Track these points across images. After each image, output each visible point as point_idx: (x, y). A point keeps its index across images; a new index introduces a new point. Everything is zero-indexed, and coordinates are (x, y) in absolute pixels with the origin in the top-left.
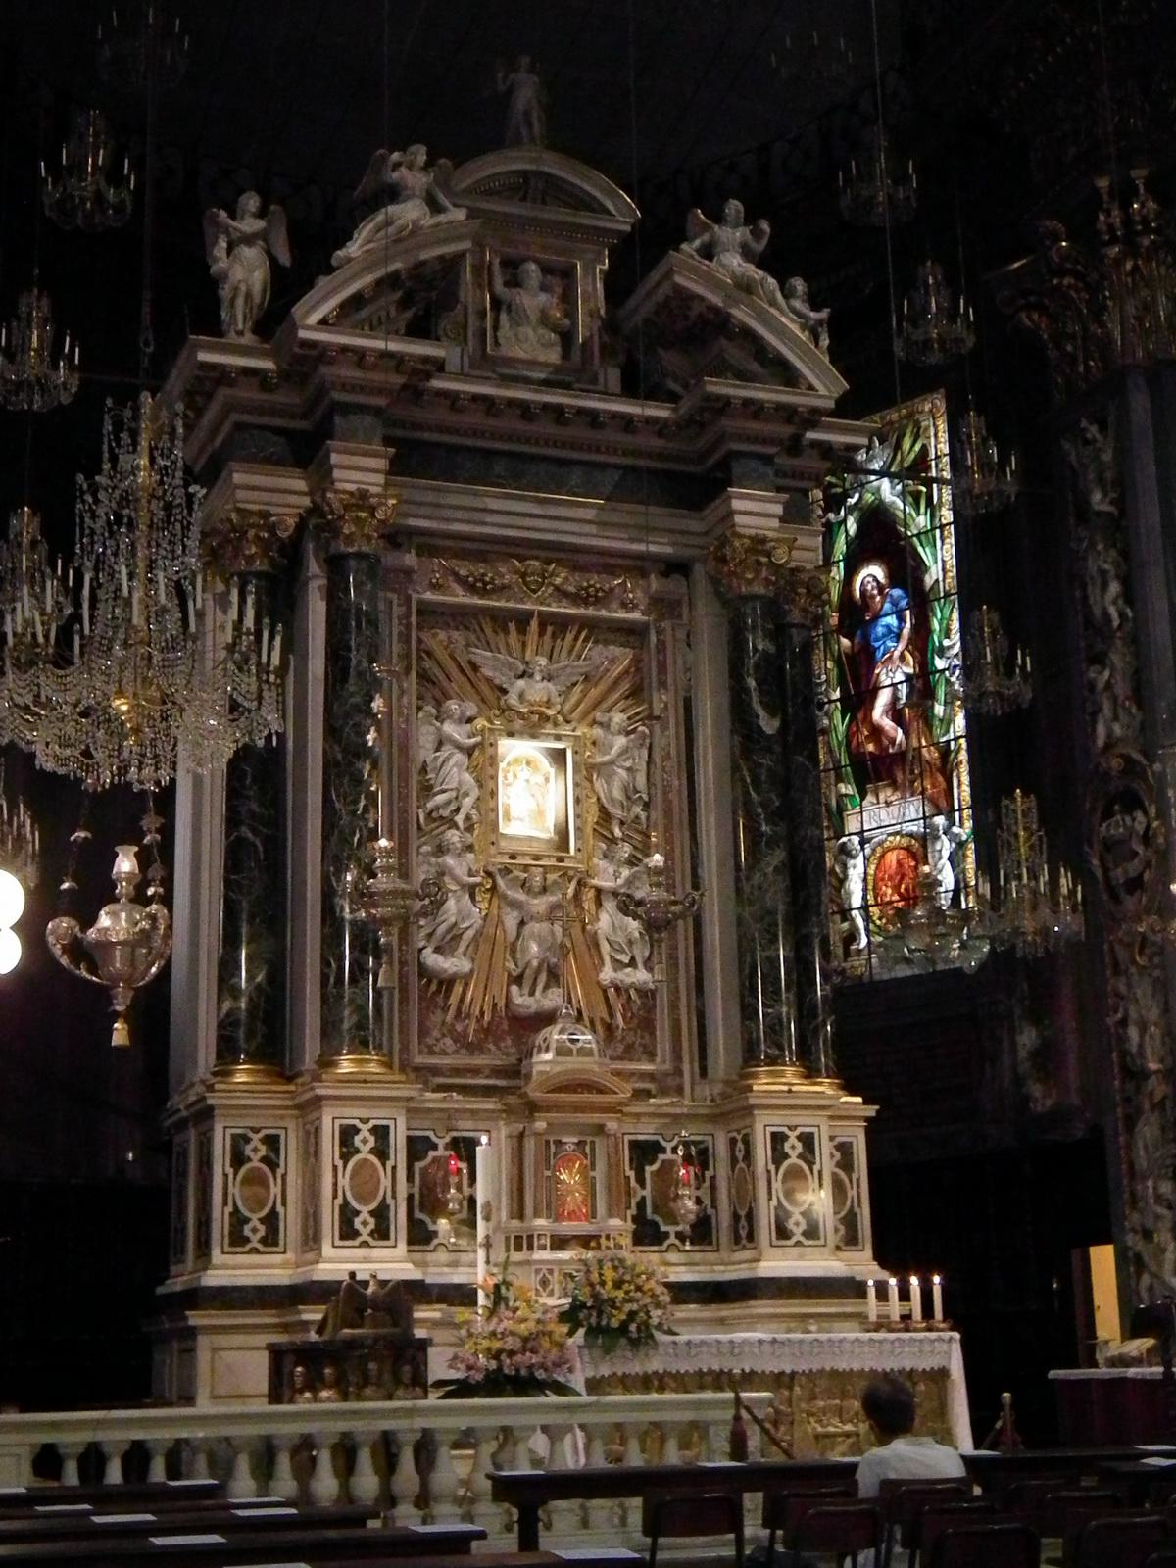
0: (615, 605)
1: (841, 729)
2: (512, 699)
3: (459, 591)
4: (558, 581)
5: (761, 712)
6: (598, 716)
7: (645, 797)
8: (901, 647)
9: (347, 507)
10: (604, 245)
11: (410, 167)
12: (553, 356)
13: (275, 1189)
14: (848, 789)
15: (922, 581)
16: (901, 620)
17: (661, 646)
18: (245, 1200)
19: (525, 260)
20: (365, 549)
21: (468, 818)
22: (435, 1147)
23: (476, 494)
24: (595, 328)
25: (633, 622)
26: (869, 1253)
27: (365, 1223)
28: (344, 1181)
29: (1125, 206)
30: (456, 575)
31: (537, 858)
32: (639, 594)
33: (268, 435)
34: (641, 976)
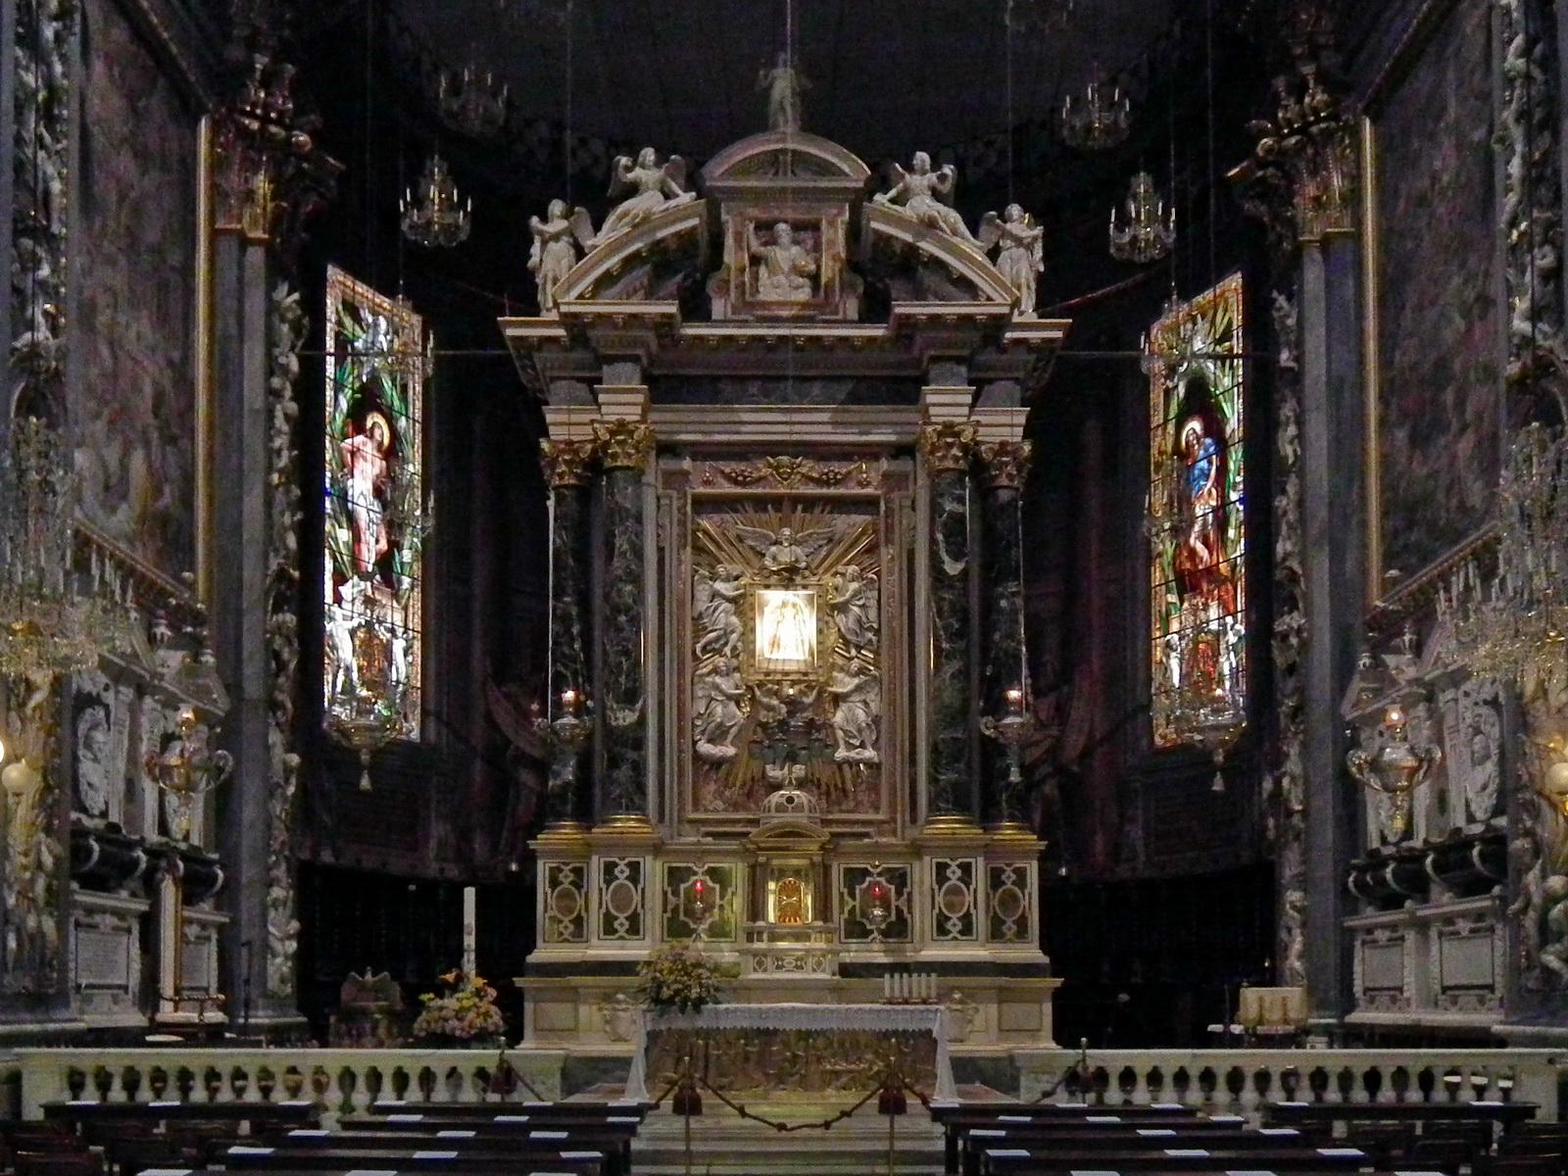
0: (852, 484)
1: (1170, 551)
2: (768, 562)
3: (726, 484)
4: (804, 470)
5: (946, 558)
6: (840, 568)
7: (875, 626)
8: (1209, 484)
9: (613, 433)
10: (846, 200)
11: (643, 167)
12: (804, 295)
13: (581, 902)
14: (1173, 598)
15: (1223, 431)
16: (1210, 463)
17: (889, 512)
18: (946, 906)
19: (777, 221)
20: (626, 462)
21: (734, 648)
22: (695, 873)
23: (733, 411)
24: (837, 269)
25: (867, 496)
26: (1036, 943)
27: (622, 925)
28: (607, 897)
29: (1300, 101)
30: (722, 472)
31: (787, 674)
32: (873, 474)
33: (573, 382)
34: (869, 753)
